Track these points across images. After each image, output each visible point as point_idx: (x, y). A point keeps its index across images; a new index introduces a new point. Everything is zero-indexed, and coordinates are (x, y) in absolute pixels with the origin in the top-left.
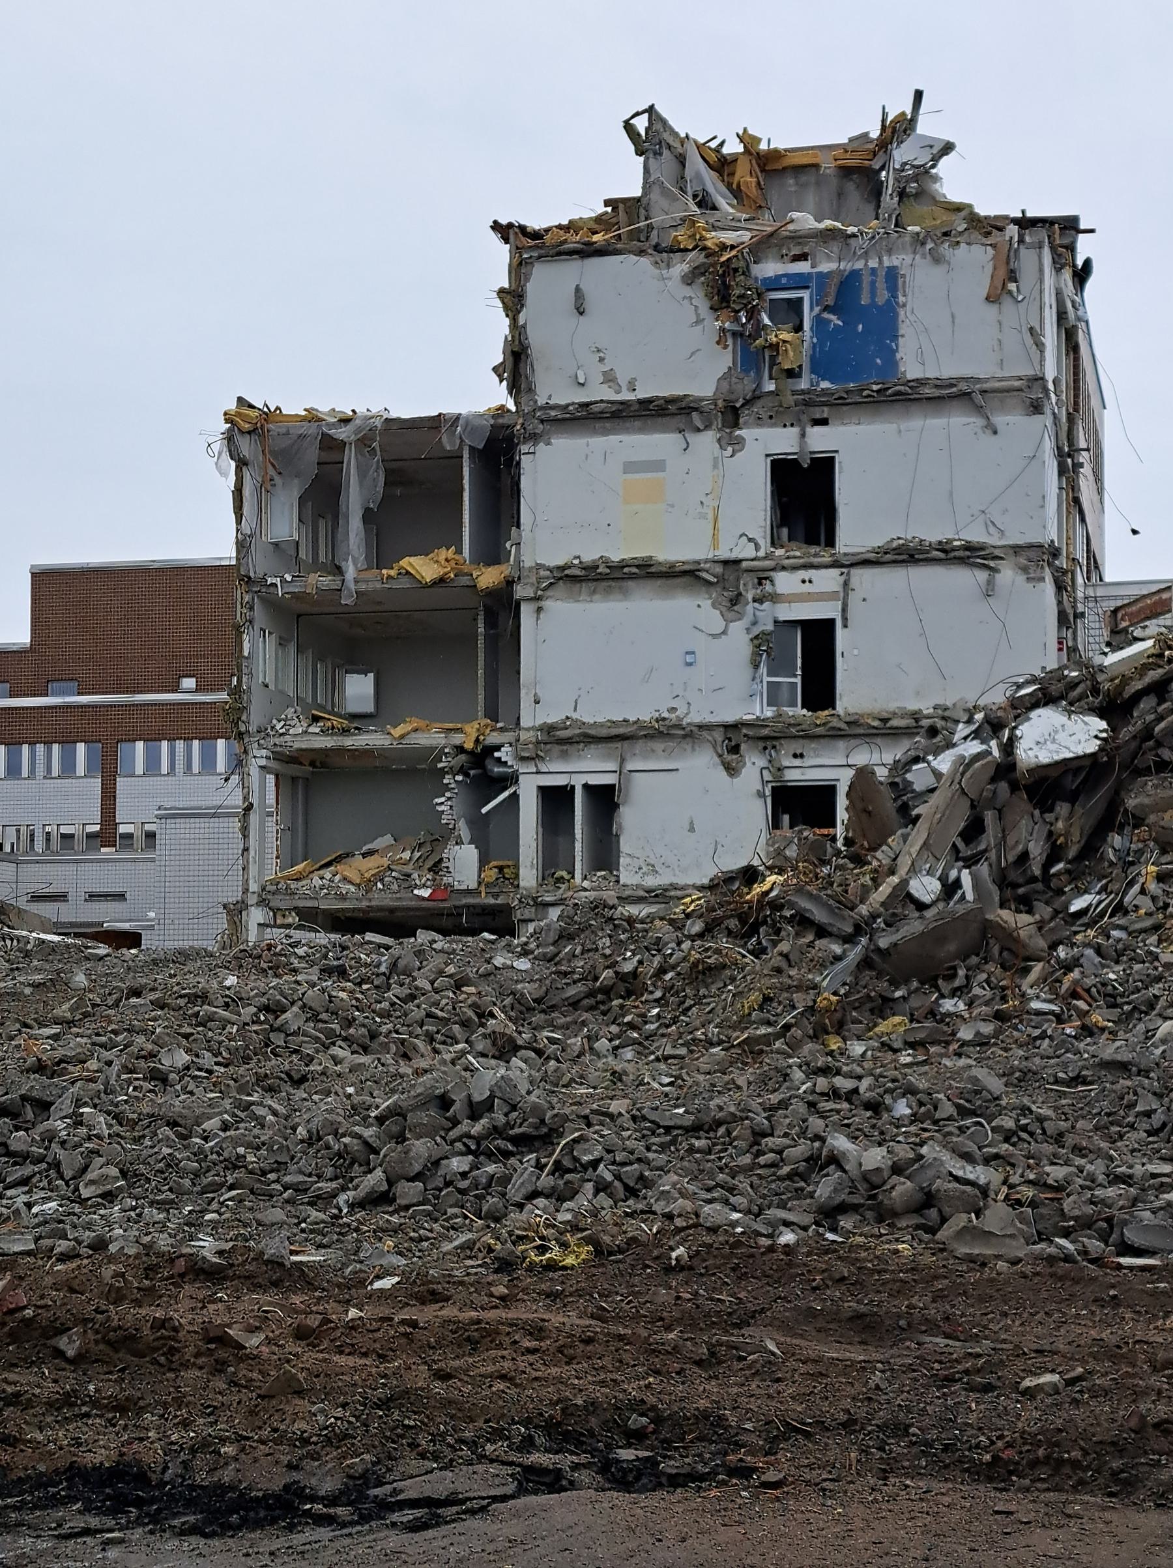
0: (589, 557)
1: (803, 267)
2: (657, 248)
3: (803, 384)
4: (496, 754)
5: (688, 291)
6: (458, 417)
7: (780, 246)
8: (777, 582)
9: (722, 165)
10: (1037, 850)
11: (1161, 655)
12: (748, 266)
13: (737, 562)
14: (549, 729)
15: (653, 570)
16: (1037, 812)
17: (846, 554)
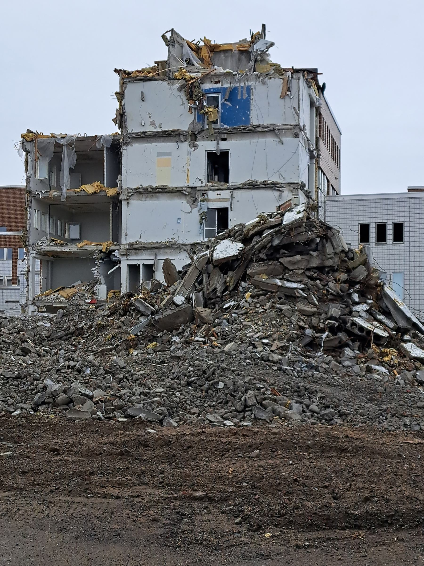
0: (145, 186)
1: (218, 86)
2: (170, 79)
3: (218, 126)
4: (113, 253)
5: (179, 93)
6: (101, 137)
7: (211, 78)
8: (209, 195)
9: (197, 50)
10: (220, 288)
11: (260, 222)
12: (199, 85)
13: (196, 188)
14: (131, 245)
15: (166, 190)
16: (222, 275)
17: (232, 185)
